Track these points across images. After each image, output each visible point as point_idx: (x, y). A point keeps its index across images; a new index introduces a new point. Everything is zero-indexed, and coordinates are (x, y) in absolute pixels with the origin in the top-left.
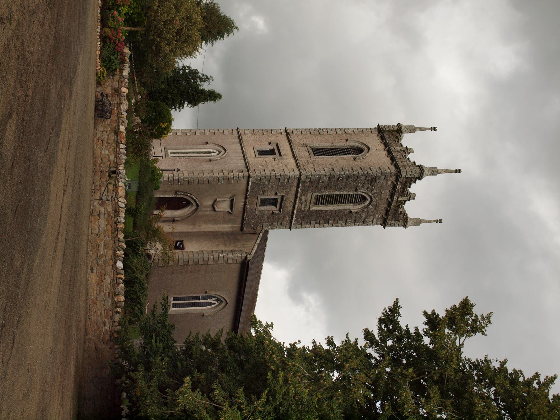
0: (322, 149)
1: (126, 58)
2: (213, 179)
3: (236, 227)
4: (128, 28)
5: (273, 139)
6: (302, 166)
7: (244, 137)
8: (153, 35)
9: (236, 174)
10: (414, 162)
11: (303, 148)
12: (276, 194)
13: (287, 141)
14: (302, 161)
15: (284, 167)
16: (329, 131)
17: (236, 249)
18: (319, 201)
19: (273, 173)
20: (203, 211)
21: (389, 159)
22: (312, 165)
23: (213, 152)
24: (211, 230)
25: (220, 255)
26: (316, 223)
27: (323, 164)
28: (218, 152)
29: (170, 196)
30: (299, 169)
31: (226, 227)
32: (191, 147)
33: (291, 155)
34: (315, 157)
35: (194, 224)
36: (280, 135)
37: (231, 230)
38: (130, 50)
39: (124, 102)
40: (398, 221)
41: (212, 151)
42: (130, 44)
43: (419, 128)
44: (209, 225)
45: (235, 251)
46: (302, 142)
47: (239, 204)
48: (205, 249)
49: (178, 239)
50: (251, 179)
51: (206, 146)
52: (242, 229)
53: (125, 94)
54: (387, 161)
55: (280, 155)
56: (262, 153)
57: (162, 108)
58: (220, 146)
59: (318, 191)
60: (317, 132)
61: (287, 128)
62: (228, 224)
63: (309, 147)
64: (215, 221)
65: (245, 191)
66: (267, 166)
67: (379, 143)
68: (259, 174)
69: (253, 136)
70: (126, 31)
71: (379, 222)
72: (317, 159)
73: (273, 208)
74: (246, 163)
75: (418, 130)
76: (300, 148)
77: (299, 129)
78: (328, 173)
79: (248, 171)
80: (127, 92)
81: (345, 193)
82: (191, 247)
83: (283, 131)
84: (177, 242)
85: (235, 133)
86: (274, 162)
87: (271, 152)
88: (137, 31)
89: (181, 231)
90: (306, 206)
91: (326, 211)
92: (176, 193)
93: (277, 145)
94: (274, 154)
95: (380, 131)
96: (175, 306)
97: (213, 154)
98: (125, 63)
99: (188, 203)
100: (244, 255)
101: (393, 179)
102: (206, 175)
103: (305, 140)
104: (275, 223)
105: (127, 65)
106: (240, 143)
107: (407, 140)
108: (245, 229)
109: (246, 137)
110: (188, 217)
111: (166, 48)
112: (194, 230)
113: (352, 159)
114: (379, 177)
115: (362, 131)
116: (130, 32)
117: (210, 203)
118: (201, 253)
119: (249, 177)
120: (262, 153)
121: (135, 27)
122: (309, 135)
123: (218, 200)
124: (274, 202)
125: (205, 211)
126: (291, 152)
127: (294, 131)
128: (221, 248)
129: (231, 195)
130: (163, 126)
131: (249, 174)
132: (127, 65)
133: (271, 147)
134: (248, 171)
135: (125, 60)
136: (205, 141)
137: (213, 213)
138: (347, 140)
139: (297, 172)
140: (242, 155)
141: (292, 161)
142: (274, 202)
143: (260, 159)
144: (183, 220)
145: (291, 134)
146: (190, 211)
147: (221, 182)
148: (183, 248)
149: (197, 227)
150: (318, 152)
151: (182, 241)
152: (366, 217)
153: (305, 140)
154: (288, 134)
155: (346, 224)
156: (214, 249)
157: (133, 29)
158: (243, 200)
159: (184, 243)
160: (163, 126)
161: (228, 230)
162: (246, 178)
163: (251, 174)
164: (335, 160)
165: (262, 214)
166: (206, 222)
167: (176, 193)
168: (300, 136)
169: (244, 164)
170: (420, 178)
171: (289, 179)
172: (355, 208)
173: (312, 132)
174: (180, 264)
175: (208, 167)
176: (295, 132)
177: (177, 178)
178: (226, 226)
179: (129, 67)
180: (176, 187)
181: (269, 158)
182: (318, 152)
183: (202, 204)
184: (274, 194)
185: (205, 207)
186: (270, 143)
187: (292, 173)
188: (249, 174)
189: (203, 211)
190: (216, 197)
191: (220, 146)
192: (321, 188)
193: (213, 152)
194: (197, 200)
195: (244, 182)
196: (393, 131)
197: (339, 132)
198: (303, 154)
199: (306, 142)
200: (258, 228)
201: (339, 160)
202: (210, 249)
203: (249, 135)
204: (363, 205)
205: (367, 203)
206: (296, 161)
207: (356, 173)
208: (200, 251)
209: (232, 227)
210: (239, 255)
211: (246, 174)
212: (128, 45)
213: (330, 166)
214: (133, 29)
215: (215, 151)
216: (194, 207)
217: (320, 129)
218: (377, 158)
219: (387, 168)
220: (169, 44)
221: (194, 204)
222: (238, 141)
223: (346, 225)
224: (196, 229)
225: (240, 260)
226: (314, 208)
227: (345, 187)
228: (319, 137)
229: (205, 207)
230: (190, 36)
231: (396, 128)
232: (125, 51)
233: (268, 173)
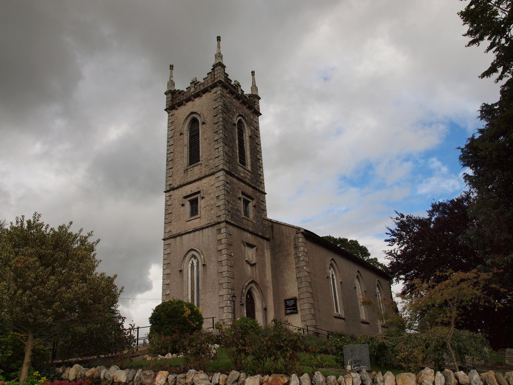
0: (190, 156)
1: (88, 373)
2: (229, 262)
3: (267, 245)
4: (25, 370)
5: (177, 203)
6: (212, 171)
7: (174, 232)
8: (45, 315)
9: (223, 236)
10: (208, 74)
11: (189, 172)
12: (240, 198)
13: (180, 189)
14: (205, 171)
15: (214, 187)
16: (170, 152)
17: (292, 244)
18: (243, 162)
19: (222, 197)
20: (256, 277)
21: (204, 95)
22: (210, 162)
23: (192, 264)
24: (270, 271)
25: (301, 259)
26: (260, 170)
27: (210, 151)
28: (193, 259)
29: (245, 311)
30: (217, 172)
31: (267, 255)
32: (185, 288)
33: (197, 183)
34: (201, 159)
35: (267, 287)
36: (173, 197)
37: (269, 250)
38: (71, 365)
39: (189, 380)
40: (255, 102)
41: (190, 265)
42: (59, 365)
43: (170, 78)
44: (267, 272)
45: (295, 245)
46: (182, 174)
47: (249, 237)
48: (294, 276)
49: (283, 306)
50: (229, 221)
51: (185, 272)
52: (268, 240)
53: (171, 377)
54: (206, 97)
55: (199, 192)
56: (194, 212)
57: (162, 313)
58: (185, 256)
59: (237, 158)
60: (171, 162)
61: (164, 190)
62: (265, 253)
63: (189, 167)
64: (263, 265)
65: (239, 230)
66: (211, 205)
67: (185, 107)
68: (223, 212)
69: (173, 223)
70: (29, 374)
71: (257, 117)
72: (204, 157)
73: (250, 205)
74: (207, 227)
75: (172, 79)
76: (189, 175)
77: (166, 180)
78: (222, 144)
79: (219, 223)
80: (165, 373)
81: (237, 135)
82: (292, 290)
83: (168, 194)
84: (287, 306)
85: (168, 242)
86: (207, 198)
87: (194, 203)
88: (33, 351)
89: (272, 301)
90: (247, 174)
91: (251, 158)
92: (242, 305)
93: (185, 197)
94: (196, 200)
95: (171, 108)
96: (337, 311)
97: (195, 264)
98: (99, 378)
99: (250, 293)
100: (300, 235)
101: (225, 91)
102: (225, 268)
103: (180, 172)
104: (262, 207)
105: (103, 372)
106: (181, 235)
107: (181, 85)
108: (268, 236)
109: (173, 230)
110: (263, 295)
111: (77, 289)
112: (271, 288)
113: (204, 125)
114: (224, 101)
115: (171, 123)
116: (34, 365)
117: (249, 268)
118: (299, 279)
119: (227, 222)
120: (194, 212)
121: (23, 355)
122: (173, 170)
123: (247, 259)
124: (246, 203)
125: (256, 274)
126: (194, 184)
127: (168, 184)
128: (292, 259)
129: (242, 245)
130: (189, 312)
131: (223, 222)
132: (103, 372)
133: (188, 204)
134: (219, 223)
135: (91, 378)
136: (178, 274)
137: (257, 266)
138: (181, 134)
139: (221, 173)
140: (197, 232)
141: (204, 181)
142: (246, 203)
143: (203, 213)
144: (264, 299)
145: (172, 186)
146: (257, 290)
147: (231, 253)
148: (295, 299)
149: (268, 285)
150: (194, 157)
151: (286, 301)
152: (254, 126)
153: (180, 172)
154: (173, 189)
155: (259, 144)
156: (294, 266)
157: (27, 359)
158: (246, 233)
159: (287, 298)
160: (189, 312)
161: (269, 253)
162: (228, 226)
163: (223, 219)
164: (205, 141)
165: (256, 217)
166: (265, 276)
167: (242, 305)
168: (175, 177)
169: (210, 228)
170: (224, 67)
171: (227, 183)
172: (247, 133)
173: (170, 167)
174: (312, 302)
175: (212, 268)
176: (170, 182)
177: (229, 302)
178: (266, 255)
179: (108, 367)
180: (237, 305)
181: (201, 203)
182: (194, 157)
183: (250, 277)
184: (239, 201)
185: (253, 274)
186: (183, 205)
187: (221, 178)
188: (223, 222)
189: (256, 277)
190: (244, 261)
191: (185, 256)
192: (233, 155)
193: (192, 264)
194: (248, 282)
195: (231, 228)
196: (172, 98)
197: (171, 142)
198: (197, 171)
199: (182, 171)
200: (266, 224)
201: (205, 137)
202: (295, 270)
203: (171, 227)
204: (245, 125)
205: (243, 121)
206: (206, 176)
207: (221, 119)
208: (297, 280)
209: (267, 249)
210: (301, 240)
211: (223, 225)
212: (61, 370)
213: (212, 144)
214: (27, 359)
215: (191, 262)
216: (253, 285)
217: (167, 160)
218: (203, 106)
219: (215, 94)
220: (67, 283)
221: (251, 285)
222: (178, 238)
223: (260, 145)
224: (270, 285)
225: (304, 240)
226: (249, 168)
227: (232, 133)
228: (176, 160)
229: (253, 274)
230: (57, 242)
231: (170, 95)
232: (72, 377)
233: (221, 203)
